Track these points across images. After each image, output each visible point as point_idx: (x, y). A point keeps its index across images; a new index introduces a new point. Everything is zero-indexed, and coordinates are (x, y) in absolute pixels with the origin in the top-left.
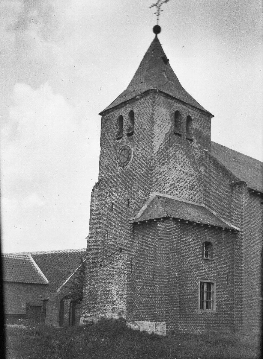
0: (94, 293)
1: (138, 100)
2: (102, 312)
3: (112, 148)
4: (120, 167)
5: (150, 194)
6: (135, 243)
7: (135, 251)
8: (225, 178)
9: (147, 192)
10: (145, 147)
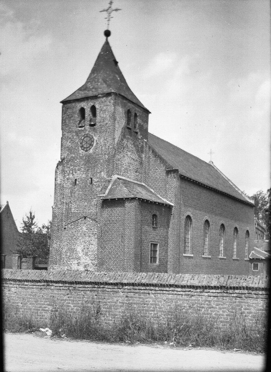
0: (59, 250)
1: (100, 98)
2: (68, 265)
3: (74, 134)
4: (82, 151)
5: (112, 176)
6: (104, 214)
7: (104, 220)
8: (162, 165)
9: (110, 175)
10: (107, 138)
